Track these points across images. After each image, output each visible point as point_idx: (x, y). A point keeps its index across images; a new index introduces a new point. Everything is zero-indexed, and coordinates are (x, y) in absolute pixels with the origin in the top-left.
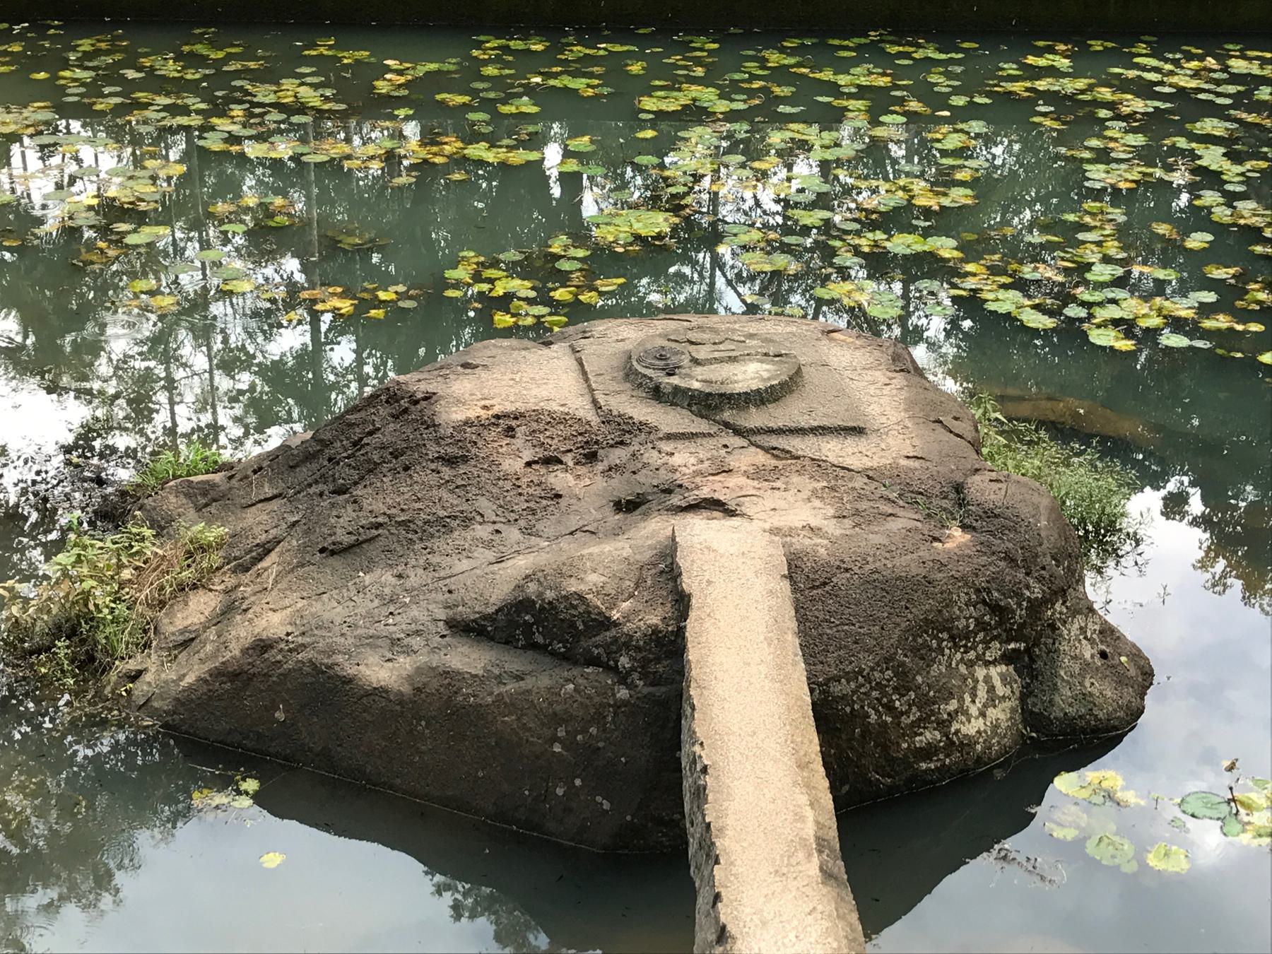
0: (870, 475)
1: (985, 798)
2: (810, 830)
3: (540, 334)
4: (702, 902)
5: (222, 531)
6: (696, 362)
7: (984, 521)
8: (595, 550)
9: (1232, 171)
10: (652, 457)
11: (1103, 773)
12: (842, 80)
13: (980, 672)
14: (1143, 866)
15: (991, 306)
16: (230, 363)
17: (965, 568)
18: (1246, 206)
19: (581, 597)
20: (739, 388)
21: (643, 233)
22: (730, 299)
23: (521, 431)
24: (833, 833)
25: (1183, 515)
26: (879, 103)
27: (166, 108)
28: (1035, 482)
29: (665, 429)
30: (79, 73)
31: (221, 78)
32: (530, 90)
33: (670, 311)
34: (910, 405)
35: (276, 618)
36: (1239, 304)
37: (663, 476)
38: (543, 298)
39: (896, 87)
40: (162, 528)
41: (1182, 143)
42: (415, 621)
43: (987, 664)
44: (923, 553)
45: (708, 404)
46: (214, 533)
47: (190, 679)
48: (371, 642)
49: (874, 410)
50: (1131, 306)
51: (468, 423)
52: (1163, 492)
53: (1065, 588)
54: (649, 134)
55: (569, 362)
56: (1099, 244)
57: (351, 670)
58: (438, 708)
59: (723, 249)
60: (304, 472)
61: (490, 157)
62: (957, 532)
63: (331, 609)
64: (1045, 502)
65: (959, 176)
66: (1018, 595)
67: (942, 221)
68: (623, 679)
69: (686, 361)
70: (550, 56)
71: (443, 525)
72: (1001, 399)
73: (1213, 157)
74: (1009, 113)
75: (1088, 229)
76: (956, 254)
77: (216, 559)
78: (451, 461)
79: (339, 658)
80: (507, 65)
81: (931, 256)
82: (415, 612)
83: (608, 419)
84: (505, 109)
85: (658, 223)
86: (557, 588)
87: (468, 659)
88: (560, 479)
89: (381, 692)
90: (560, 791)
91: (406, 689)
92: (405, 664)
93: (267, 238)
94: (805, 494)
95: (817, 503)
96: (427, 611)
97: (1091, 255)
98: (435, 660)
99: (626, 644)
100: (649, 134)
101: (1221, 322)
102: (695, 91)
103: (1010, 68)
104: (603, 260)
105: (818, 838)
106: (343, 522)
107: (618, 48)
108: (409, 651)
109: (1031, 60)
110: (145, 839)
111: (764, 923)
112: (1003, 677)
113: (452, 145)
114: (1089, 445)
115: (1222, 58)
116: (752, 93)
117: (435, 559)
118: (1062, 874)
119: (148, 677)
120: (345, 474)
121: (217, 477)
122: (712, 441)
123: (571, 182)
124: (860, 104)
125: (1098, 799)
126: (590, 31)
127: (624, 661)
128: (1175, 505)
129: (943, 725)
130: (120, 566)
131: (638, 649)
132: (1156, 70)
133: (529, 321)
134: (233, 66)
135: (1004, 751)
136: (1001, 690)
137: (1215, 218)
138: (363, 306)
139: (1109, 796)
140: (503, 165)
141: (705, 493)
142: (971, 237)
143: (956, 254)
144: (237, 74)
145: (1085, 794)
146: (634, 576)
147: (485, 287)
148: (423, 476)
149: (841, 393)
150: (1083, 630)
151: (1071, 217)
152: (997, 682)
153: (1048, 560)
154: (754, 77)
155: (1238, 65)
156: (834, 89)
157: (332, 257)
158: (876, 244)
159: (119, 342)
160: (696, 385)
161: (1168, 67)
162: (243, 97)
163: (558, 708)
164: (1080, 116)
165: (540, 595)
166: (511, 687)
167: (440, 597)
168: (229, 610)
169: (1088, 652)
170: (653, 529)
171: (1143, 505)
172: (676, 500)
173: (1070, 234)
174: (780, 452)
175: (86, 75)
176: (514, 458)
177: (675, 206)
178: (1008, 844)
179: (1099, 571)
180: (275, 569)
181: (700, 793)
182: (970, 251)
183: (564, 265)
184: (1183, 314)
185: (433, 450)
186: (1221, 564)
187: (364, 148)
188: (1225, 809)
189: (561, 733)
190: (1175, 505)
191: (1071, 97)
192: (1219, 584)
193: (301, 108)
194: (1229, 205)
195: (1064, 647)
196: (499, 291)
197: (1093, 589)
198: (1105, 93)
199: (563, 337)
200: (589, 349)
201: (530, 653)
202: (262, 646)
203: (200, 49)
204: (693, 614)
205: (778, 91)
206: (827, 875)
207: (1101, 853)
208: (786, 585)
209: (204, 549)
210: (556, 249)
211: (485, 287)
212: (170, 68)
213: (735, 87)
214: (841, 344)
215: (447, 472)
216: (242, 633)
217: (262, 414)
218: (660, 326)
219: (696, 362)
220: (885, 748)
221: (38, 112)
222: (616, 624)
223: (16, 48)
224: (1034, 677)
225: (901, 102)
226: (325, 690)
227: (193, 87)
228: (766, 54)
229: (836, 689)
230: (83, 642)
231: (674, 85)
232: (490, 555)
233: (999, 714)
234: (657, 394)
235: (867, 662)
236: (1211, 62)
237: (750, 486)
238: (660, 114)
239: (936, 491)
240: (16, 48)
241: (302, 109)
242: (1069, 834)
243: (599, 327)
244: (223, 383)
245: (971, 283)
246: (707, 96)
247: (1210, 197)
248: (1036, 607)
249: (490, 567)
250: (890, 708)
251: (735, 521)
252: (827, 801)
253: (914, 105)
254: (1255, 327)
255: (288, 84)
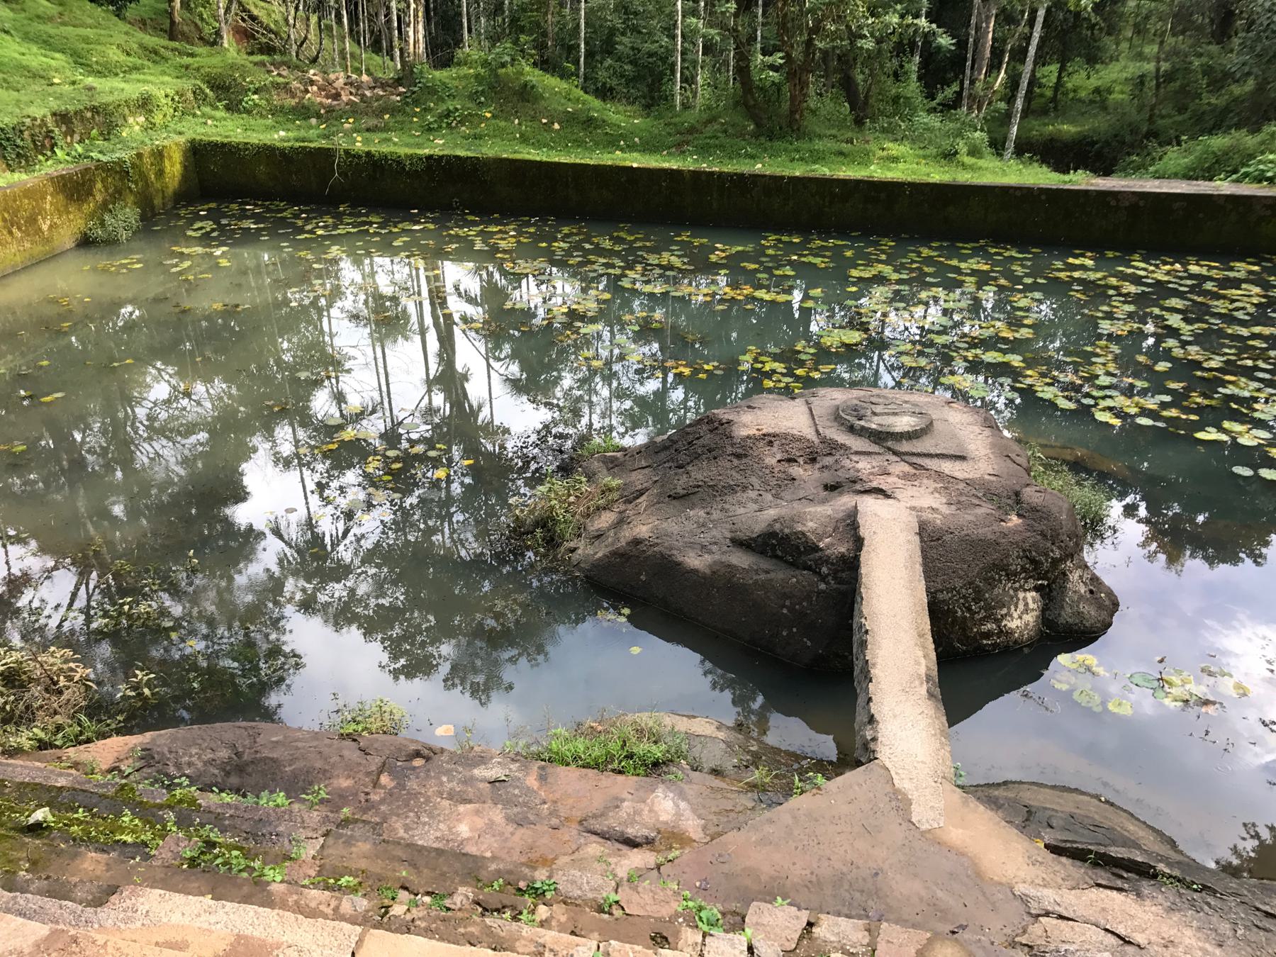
0: (968, 482)
1: (1022, 663)
2: (923, 670)
3: (788, 393)
4: (861, 701)
5: (620, 481)
6: (874, 414)
7: (1031, 513)
8: (812, 509)
9: (1186, 328)
10: (846, 463)
11: (1084, 656)
12: (963, 265)
13: (1021, 595)
14: (1106, 710)
15: (1040, 395)
16: (620, 394)
17: (1017, 538)
18: (1193, 349)
19: (803, 534)
20: (898, 430)
21: (847, 342)
22: (886, 379)
23: (776, 444)
24: (935, 673)
25: (1134, 516)
26: (983, 280)
27: (604, 264)
28: (1059, 493)
29: (855, 449)
30: (562, 245)
31: (632, 250)
32: (791, 263)
33: (853, 384)
34: (993, 446)
35: (644, 528)
36: (1185, 403)
37: (852, 473)
38: (790, 373)
39: (993, 271)
40: (591, 477)
41: (1156, 311)
42: (714, 537)
43: (1025, 590)
44: (995, 528)
45: (880, 437)
46: (616, 482)
47: (600, 555)
48: (691, 545)
49: (972, 447)
50: (1120, 401)
51: (748, 437)
52: (1124, 503)
53: (1073, 553)
54: (854, 289)
55: (804, 409)
56: (1104, 364)
57: (680, 559)
58: (721, 583)
59: (886, 355)
60: (662, 456)
61: (767, 297)
62: (1015, 518)
63: (672, 526)
64: (1066, 505)
65: (1026, 322)
66: (1046, 555)
67: (1015, 346)
68: (823, 579)
69: (869, 413)
70: (802, 246)
71: (732, 489)
72: (1043, 446)
73: (1175, 320)
74: (1056, 288)
75: (1098, 355)
76: (1022, 365)
77: (615, 495)
78: (739, 456)
79: (675, 552)
80: (780, 249)
81: (1006, 365)
82: (714, 532)
83: (824, 441)
84: (777, 272)
85: (854, 337)
86: (791, 527)
87: (741, 560)
88: (796, 471)
89: (695, 571)
90: (785, 633)
91: (708, 571)
92: (708, 558)
93: (646, 332)
94: (931, 490)
95: (937, 495)
96: (721, 533)
97: (1099, 371)
98: (724, 558)
99: (827, 561)
100: (854, 289)
101: (1173, 413)
102: (881, 267)
103: (1059, 264)
104: (824, 354)
105: (927, 675)
106: (681, 483)
107: (840, 243)
108: (710, 552)
109: (1071, 260)
110: (561, 629)
111: (895, 716)
112: (1033, 598)
113: (747, 290)
114: (1091, 475)
115: (1184, 265)
116: (912, 270)
117: (727, 506)
118: (1058, 708)
119: (579, 551)
120: (683, 458)
121: (619, 454)
122: (881, 457)
123: (806, 313)
124: (972, 279)
125: (1082, 670)
126: (825, 233)
127: (824, 570)
128: (1130, 511)
129: (998, 621)
130: (569, 495)
131: (832, 564)
132: (1145, 269)
133: (782, 385)
134: (638, 244)
135: (1030, 638)
136: (1031, 605)
137: (1173, 354)
138: (696, 372)
139: (1089, 669)
140: (773, 302)
141: (874, 484)
142: (1030, 355)
143: (1022, 365)
144: (640, 248)
145: (1074, 666)
146: (833, 525)
147: (760, 366)
148: (723, 463)
149: (954, 436)
150: (1081, 577)
151: (1089, 349)
152: (1030, 601)
153: (1065, 537)
154: (913, 262)
155: (1194, 269)
156: (957, 270)
157: (675, 343)
158: (976, 356)
159: (568, 381)
160: (874, 426)
161: (1152, 268)
162: (642, 260)
163: (787, 590)
164: (1097, 292)
165: (782, 530)
166: (763, 576)
167: (728, 526)
168: (621, 522)
169: (1083, 589)
170: (845, 501)
171: (1115, 508)
172: (858, 487)
173: (1088, 358)
174: (918, 466)
175: (565, 245)
176: (772, 458)
177: (864, 327)
178: (1028, 688)
179: (1091, 545)
180: (644, 504)
181: (863, 644)
182: (1030, 363)
183: (803, 357)
184: (1151, 407)
185: (729, 450)
186: (1154, 546)
187: (699, 291)
188: (1156, 684)
189: (788, 603)
190: (1130, 511)
191: (1093, 282)
192: (1151, 557)
193: (670, 267)
194: (1183, 347)
195: (1069, 585)
196: (767, 368)
197: (1088, 556)
198: (1113, 281)
199: (801, 395)
200: (815, 402)
201: (774, 561)
202: (637, 542)
203: (622, 234)
204: (865, 549)
205: (926, 269)
206: (931, 695)
207: (1083, 700)
208: (917, 538)
209: (610, 490)
210: (799, 348)
211: (760, 366)
212: (607, 244)
213: (903, 266)
214: (956, 410)
215: (736, 462)
216: (627, 534)
217: (635, 422)
218: (856, 393)
219: (874, 414)
220: (964, 630)
221: (540, 263)
222: (821, 550)
223: (532, 230)
224: (1051, 600)
225: (995, 279)
226: (667, 567)
227: (617, 254)
228: (921, 249)
229: (940, 596)
230: (549, 531)
231: (869, 264)
232: (756, 507)
233: (1030, 618)
234: (851, 429)
235: (958, 583)
236: (1178, 266)
237: (900, 483)
238: (860, 279)
239: (1005, 494)
240: (532, 230)
241: (671, 268)
242: (1064, 687)
243: (822, 391)
244: (616, 405)
245: (1029, 381)
246: (887, 270)
247: (1171, 343)
248: (1056, 562)
249: (758, 512)
250: (969, 609)
251: (890, 501)
252: (933, 655)
253: (1002, 282)
254: (1193, 417)
255: (665, 255)
